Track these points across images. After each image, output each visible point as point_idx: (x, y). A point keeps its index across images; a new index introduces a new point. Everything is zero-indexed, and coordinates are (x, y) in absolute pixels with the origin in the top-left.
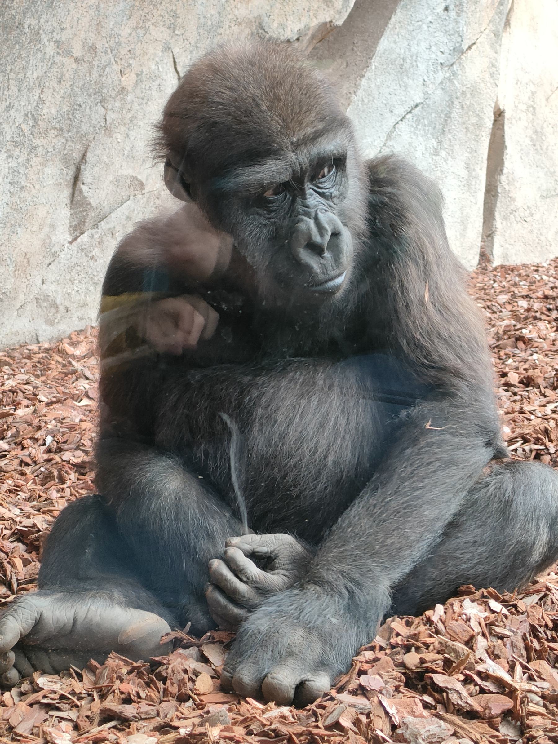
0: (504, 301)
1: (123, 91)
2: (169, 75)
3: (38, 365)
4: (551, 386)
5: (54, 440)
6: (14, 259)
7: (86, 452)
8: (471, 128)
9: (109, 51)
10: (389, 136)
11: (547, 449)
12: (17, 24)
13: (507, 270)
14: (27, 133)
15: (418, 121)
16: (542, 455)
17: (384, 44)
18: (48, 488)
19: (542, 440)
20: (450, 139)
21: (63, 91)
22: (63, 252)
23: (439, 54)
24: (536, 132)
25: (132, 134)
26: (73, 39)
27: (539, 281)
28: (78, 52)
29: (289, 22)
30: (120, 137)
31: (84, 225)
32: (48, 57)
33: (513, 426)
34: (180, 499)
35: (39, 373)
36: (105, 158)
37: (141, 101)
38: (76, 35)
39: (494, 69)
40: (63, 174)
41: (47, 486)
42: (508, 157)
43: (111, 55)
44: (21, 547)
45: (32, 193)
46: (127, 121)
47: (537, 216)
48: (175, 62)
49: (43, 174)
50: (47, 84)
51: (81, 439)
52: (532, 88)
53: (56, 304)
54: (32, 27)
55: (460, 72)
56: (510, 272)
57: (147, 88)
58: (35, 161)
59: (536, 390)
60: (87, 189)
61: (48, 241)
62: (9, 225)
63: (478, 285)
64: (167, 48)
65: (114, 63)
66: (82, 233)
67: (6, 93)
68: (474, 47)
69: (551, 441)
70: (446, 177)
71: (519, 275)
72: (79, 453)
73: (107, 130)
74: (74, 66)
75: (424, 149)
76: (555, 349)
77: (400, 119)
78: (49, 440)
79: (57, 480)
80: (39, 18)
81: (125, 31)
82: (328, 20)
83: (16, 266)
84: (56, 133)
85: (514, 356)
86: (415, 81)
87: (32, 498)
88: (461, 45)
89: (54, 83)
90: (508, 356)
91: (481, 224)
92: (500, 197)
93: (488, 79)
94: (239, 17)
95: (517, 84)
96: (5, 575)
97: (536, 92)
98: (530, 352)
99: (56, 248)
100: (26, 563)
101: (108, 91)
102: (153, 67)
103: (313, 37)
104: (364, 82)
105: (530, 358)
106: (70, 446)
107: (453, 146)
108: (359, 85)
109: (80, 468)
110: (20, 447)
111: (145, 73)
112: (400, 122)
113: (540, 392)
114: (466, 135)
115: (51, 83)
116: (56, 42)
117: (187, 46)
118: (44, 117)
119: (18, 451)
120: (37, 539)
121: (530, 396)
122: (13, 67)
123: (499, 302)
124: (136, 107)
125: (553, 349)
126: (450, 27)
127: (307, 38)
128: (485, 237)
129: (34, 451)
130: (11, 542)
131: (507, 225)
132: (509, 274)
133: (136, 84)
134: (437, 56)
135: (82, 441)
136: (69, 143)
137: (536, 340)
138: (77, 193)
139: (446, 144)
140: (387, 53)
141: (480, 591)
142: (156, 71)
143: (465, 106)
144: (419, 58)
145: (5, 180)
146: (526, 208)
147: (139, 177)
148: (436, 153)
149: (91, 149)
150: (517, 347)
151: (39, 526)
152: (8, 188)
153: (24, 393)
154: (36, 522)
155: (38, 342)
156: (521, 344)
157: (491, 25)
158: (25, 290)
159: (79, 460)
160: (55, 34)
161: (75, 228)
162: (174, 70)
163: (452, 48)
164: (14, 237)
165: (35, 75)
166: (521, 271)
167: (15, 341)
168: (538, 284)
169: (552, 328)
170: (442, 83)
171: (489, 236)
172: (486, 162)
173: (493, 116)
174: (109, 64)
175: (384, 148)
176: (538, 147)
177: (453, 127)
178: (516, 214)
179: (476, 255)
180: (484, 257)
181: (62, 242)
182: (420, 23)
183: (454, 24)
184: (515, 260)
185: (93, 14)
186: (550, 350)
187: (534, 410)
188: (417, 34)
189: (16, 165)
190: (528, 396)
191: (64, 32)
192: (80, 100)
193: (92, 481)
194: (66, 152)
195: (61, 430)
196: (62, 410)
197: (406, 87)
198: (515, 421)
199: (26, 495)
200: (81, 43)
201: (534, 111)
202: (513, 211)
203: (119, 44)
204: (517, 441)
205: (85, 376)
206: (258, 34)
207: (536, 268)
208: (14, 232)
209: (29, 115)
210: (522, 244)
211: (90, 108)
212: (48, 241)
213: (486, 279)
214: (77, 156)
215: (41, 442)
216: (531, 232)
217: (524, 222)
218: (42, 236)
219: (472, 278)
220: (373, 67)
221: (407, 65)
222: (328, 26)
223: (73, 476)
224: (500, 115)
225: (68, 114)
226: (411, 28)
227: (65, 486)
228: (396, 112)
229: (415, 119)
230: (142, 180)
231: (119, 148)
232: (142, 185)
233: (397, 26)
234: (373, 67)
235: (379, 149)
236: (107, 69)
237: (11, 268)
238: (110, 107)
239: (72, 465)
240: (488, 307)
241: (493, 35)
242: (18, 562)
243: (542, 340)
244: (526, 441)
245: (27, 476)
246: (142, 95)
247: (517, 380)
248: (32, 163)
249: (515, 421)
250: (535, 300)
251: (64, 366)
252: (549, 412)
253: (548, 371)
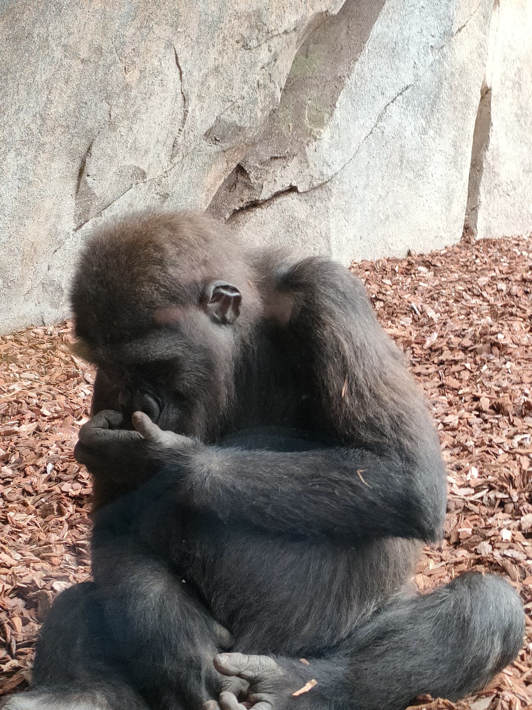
0: (485, 283)
1: (127, 87)
2: (171, 71)
3: (42, 360)
4: (519, 414)
5: (54, 469)
6: (21, 249)
7: (85, 485)
8: (459, 107)
9: (114, 50)
10: (380, 118)
11: (510, 497)
12: (26, 35)
13: (489, 243)
14: (35, 131)
15: (408, 103)
16: (506, 503)
17: (377, 29)
18: (48, 522)
19: (506, 488)
20: (438, 119)
21: (69, 91)
22: (68, 240)
23: (430, 37)
24: (521, 108)
25: (135, 127)
26: (79, 42)
27: (519, 257)
28: (84, 53)
29: (287, 14)
30: (124, 131)
31: (88, 213)
32: (56, 61)
33: (481, 466)
34: (163, 602)
35: (43, 370)
36: (109, 151)
37: (144, 96)
38: (83, 38)
39: (482, 50)
40: (69, 168)
41: (47, 519)
42: (493, 133)
43: (116, 55)
44: (19, 602)
45: (39, 187)
46: (130, 115)
47: (520, 190)
48: (177, 58)
49: (50, 168)
50: (55, 85)
51: (79, 471)
52: (519, 64)
53: (61, 288)
54: (41, 35)
55: (449, 54)
56: (492, 246)
57: (150, 83)
58: (43, 157)
59: (505, 418)
60: (92, 180)
61: (54, 230)
62: (17, 218)
63: (461, 260)
64: (169, 45)
65: (119, 61)
66: (87, 221)
67: (15, 97)
68: (464, 30)
69: (514, 487)
70: (434, 155)
71: (500, 250)
72: (77, 485)
73: (112, 125)
74: (81, 67)
75: (413, 128)
76: (527, 357)
77: (391, 101)
78: (50, 467)
79: (56, 513)
80: (48, 26)
81: (130, 32)
82: (324, 10)
83: (23, 255)
84: (63, 130)
85: (488, 361)
86: (407, 64)
87: (32, 541)
88: (451, 28)
89: (61, 84)
90: (483, 362)
91: (466, 199)
92: (485, 173)
93: (476, 60)
94: (239, 11)
95: (504, 61)
96: (5, 637)
97: (522, 69)
98: (504, 360)
99: (62, 236)
100: (25, 622)
101: (113, 88)
102: (156, 63)
103: (309, 26)
104: (357, 66)
105: (503, 366)
106: (69, 476)
107: (441, 125)
108: (353, 68)
109: (78, 500)
110: (22, 474)
111: (148, 69)
112: (391, 104)
113: (509, 420)
114: (454, 114)
115: (59, 84)
116: (64, 46)
117: (189, 42)
118: (52, 116)
119: (19, 479)
120: (36, 597)
121: (500, 424)
122: (22, 73)
123: (480, 284)
124: (139, 102)
125: (526, 356)
126: (441, 12)
127: (304, 27)
128: (469, 211)
129: (35, 480)
130: (11, 598)
131: (490, 198)
132: (491, 248)
133: (140, 80)
134: (427, 39)
135: (80, 473)
136: (75, 138)
137: (510, 345)
138: (82, 184)
139: (434, 123)
140: (380, 37)
141: (437, 700)
142: (159, 67)
143: (453, 86)
144: (410, 42)
145: (14, 176)
146: (509, 182)
147: (141, 167)
148: (425, 132)
149: (95, 143)
150: (492, 353)
151: (38, 582)
152: (16, 183)
153: (28, 404)
154: (34, 578)
155: (44, 324)
156: (496, 350)
157: (480, 8)
158: (31, 277)
159: (77, 493)
160: (63, 39)
161: (80, 216)
162: (176, 65)
163: (442, 32)
164: (22, 229)
165: (44, 78)
166: (502, 245)
167: (21, 325)
168: (517, 260)
169: (526, 327)
170: (432, 65)
171: (473, 209)
172: (472, 139)
173: (480, 94)
174: (114, 63)
175: (374, 129)
176: (523, 123)
177: (442, 107)
178: (500, 189)
179: (460, 228)
180: (468, 230)
181: (67, 230)
182: (413, 8)
183: (445, 9)
184: (497, 234)
185: (100, 17)
186: (523, 358)
187: (502, 443)
188: (409, 19)
189: (25, 162)
190: (498, 424)
191: (72, 37)
192: (86, 98)
193: (88, 514)
194: (72, 147)
195: (61, 457)
196: (63, 432)
197: (397, 70)
198: (483, 461)
199: (27, 537)
200: (88, 46)
201: (520, 87)
202: (496, 186)
203: (124, 43)
204: (484, 489)
205: (86, 380)
206: (256, 26)
207: (516, 242)
208: (22, 224)
209: (38, 115)
210: (504, 217)
211: (96, 105)
212: (54, 230)
213: (469, 254)
214: (83, 149)
215: (42, 469)
216: (513, 205)
217: (507, 196)
218: (48, 226)
219: (456, 253)
220: (367, 51)
221: (399, 49)
222: (324, 15)
223: (71, 508)
224: (486, 92)
225: (74, 112)
226: (403, 13)
227: (63, 519)
228: (387, 94)
229: (405, 100)
230: (144, 169)
231: (123, 141)
232: (144, 175)
233: (390, 11)
234: (367, 51)
235: (370, 130)
236: (112, 68)
237: (19, 258)
238: (115, 103)
239: (70, 497)
240: (469, 290)
241: (482, 17)
242: (17, 621)
243: (516, 346)
244: (491, 488)
245: (28, 507)
246: (145, 91)
247: (488, 405)
248: (39, 159)
249: (483, 461)
250: (514, 283)
251: (67, 363)
252: (516, 445)
253: (518, 395)
